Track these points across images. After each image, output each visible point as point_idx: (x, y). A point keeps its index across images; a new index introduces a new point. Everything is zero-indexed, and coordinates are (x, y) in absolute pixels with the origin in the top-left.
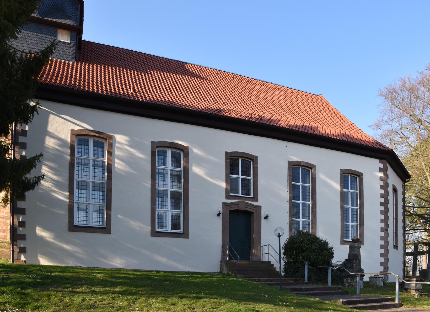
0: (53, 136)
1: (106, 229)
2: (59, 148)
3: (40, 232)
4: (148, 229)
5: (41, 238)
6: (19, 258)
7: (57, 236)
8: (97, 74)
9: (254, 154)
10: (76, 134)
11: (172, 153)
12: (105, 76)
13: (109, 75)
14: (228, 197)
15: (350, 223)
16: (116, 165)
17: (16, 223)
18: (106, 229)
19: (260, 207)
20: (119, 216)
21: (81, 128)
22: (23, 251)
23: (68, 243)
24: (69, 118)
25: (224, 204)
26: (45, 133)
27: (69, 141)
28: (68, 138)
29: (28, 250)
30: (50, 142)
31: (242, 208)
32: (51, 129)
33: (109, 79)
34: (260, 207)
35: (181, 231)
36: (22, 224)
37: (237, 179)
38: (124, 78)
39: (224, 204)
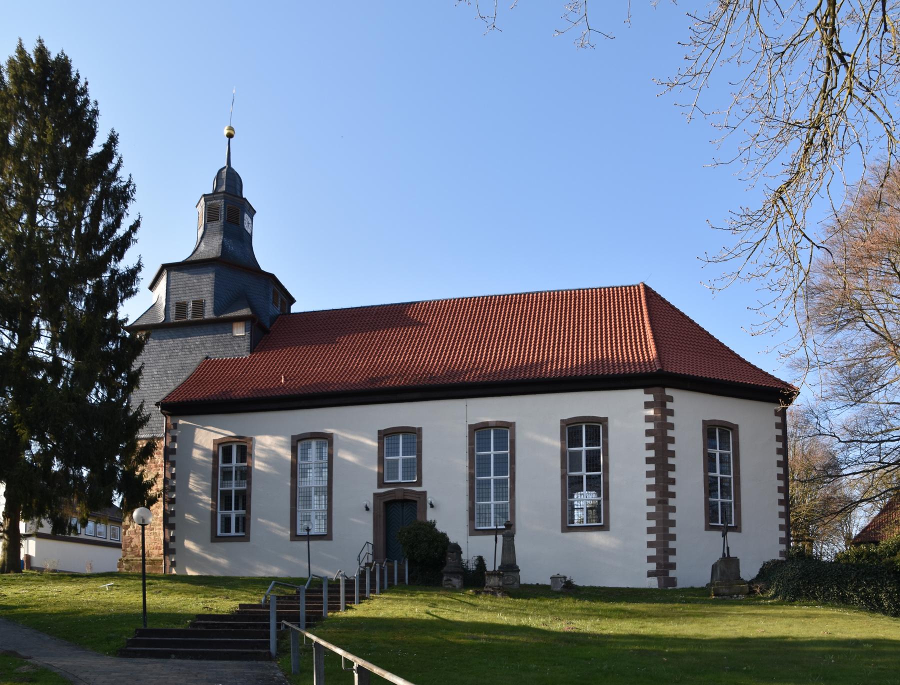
0: (199, 448)
1: (327, 536)
2: (205, 459)
3: (189, 544)
4: (287, 534)
5: (188, 550)
6: (171, 571)
7: (205, 549)
8: (625, 331)
9: (417, 426)
10: (218, 443)
11: (586, 426)
12: (550, 338)
13: (555, 335)
14: (381, 484)
15: (492, 501)
16: (256, 467)
17: (167, 537)
18: (327, 536)
19: (424, 493)
20: (259, 520)
21: (223, 436)
22: (173, 564)
23: (210, 555)
24: (211, 428)
25: (375, 494)
26: (193, 446)
27: (212, 448)
28: (210, 446)
29: (178, 564)
30: (197, 454)
31: (400, 496)
32: (197, 441)
33: (583, 339)
34: (424, 493)
35: (219, 533)
36: (173, 539)
37: (580, 452)
38: (512, 344)
39: (375, 494)
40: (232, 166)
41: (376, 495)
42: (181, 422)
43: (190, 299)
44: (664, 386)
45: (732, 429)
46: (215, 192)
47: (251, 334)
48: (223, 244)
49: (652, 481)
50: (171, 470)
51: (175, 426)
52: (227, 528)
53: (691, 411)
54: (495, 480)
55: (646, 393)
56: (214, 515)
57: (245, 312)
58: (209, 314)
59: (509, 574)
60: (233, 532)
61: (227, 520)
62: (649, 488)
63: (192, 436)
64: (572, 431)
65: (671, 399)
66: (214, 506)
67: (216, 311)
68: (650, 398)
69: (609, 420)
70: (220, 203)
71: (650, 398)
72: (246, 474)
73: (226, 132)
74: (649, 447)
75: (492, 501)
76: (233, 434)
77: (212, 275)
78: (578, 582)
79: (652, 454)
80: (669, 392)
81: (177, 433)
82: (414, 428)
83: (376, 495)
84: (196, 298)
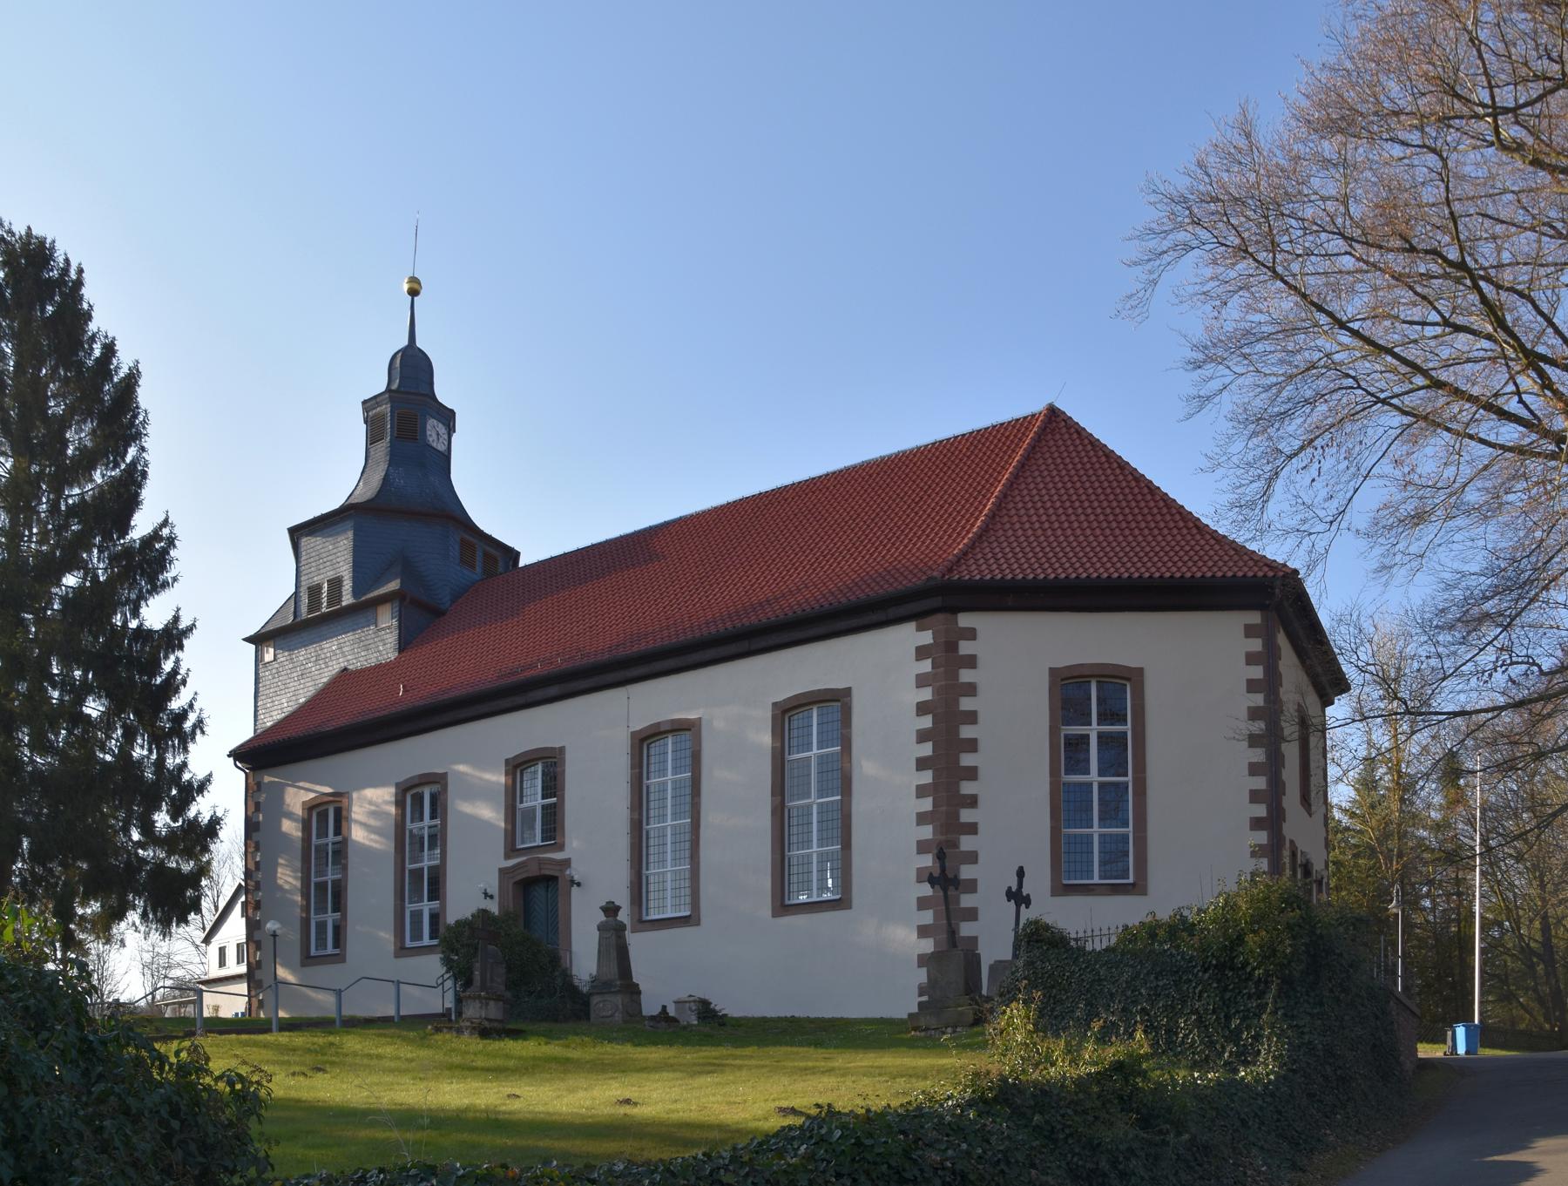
14: (511, 850)
15: (1096, 828)
21: (312, 795)
25: (501, 870)
31: (533, 871)
35: (313, 952)
39: (501, 870)
40: (419, 344)
41: (502, 871)
42: (267, 779)
43: (322, 578)
44: (955, 610)
45: (1128, 679)
46: (388, 390)
47: (400, 621)
48: (386, 480)
49: (927, 804)
50: (254, 858)
51: (259, 785)
52: (417, 935)
53: (1018, 657)
54: (1102, 786)
55: (920, 629)
56: (306, 923)
57: (394, 585)
58: (347, 599)
59: (607, 997)
60: (426, 941)
61: (321, 927)
62: (922, 818)
63: (281, 799)
64: (1072, 691)
65: (971, 634)
66: (307, 909)
67: (356, 592)
68: (927, 638)
69: (855, 693)
70: (386, 408)
71: (927, 638)
72: (341, 851)
73: (406, 287)
74: (922, 737)
75: (1096, 828)
76: (328, 790)
77: (350, 534)
78: (731, 1005)
79: (927, 749)
80: (965, 620)
81: (262, 798)
82: (553, 749)
83: (502, 871)
84: (331, 574)
